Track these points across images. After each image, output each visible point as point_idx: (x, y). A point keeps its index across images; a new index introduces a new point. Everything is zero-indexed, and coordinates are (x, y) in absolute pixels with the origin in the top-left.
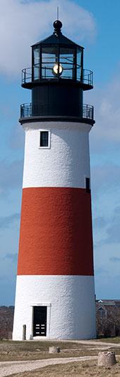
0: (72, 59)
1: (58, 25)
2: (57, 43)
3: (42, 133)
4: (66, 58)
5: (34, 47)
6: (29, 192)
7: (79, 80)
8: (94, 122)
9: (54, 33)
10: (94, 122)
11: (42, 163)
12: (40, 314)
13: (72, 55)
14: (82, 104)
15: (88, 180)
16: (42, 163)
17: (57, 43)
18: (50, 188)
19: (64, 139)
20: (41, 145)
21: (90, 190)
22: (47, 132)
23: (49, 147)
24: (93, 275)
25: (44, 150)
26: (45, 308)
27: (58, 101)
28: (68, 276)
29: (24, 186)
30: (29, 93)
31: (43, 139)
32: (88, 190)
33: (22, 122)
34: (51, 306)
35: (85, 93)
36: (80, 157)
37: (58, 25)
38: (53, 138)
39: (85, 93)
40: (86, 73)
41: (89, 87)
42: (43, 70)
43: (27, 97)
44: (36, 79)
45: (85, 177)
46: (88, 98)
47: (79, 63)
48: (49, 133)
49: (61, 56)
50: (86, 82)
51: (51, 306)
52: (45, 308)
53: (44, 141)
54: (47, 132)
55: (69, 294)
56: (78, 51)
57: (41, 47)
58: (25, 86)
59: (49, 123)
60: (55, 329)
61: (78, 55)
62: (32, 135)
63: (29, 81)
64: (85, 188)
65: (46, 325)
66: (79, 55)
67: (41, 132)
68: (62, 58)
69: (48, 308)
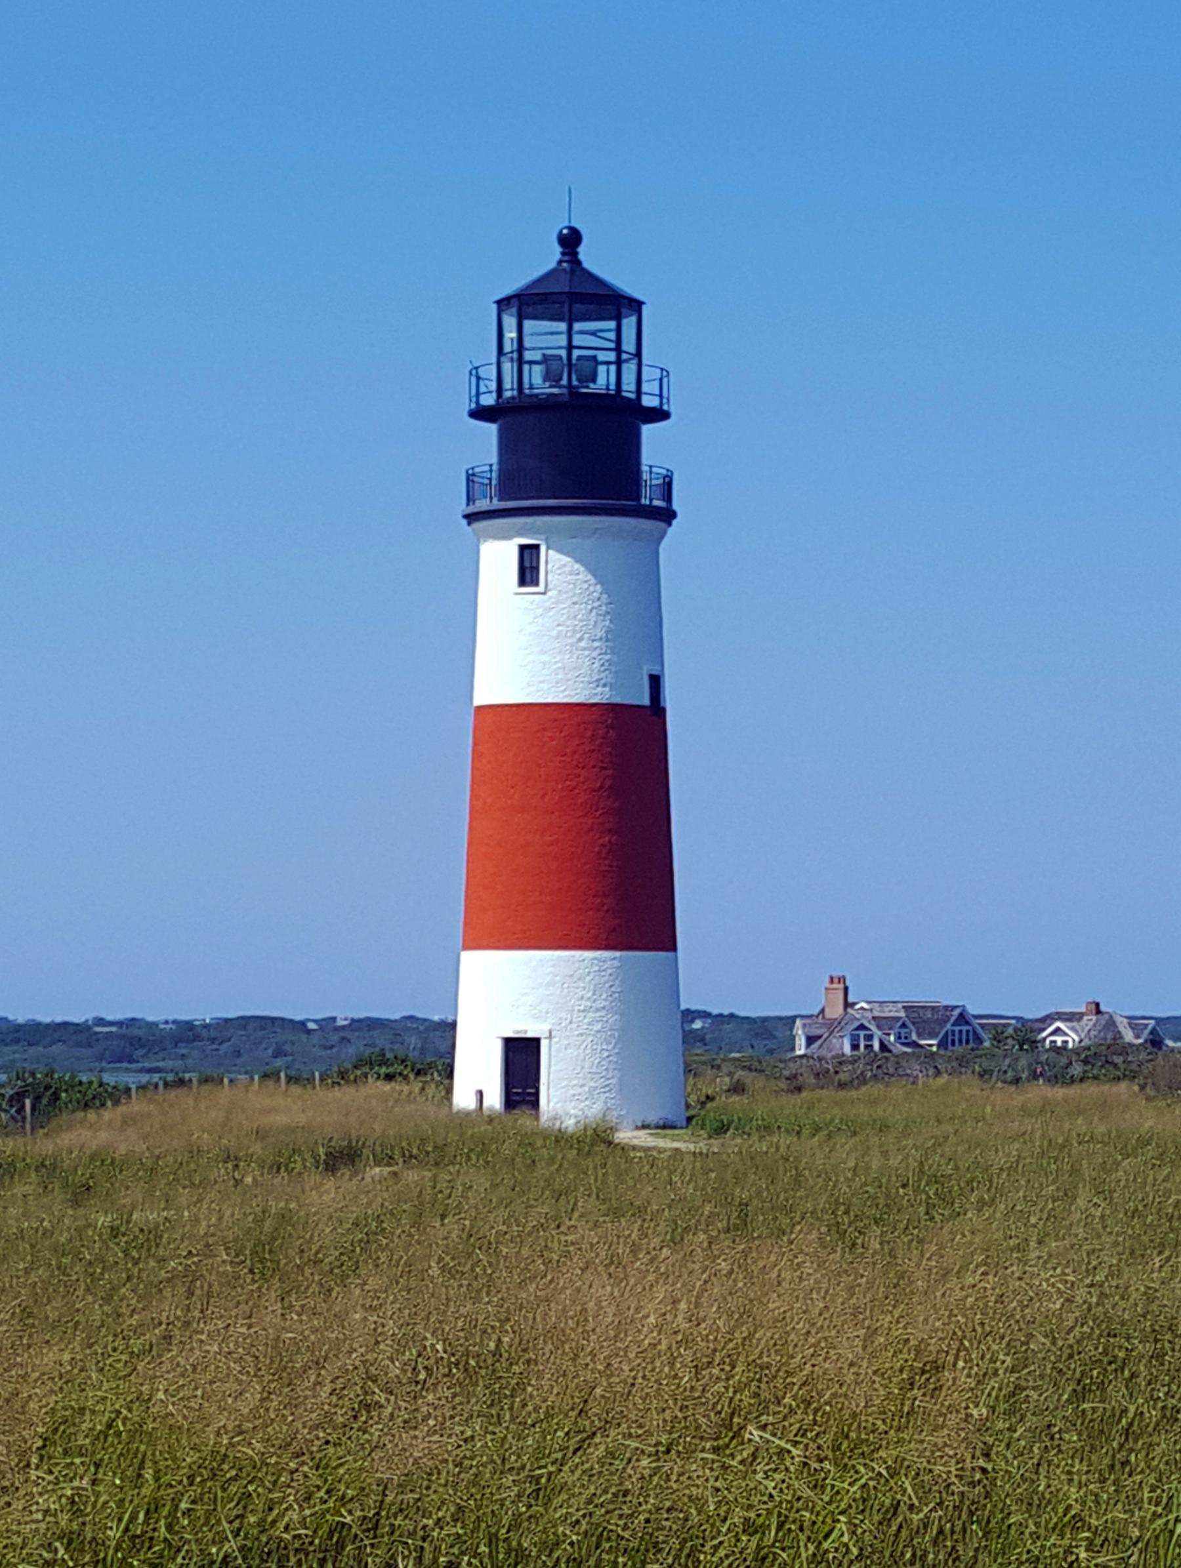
0: (612, 336)
1: (570, 240)
2: (573, 292)
3: (523, 548)
4: (593, 333)
5: (503, 304)
6: (501, 721)
7: (632, 396)
8: (673, 515)
9: (560, 262)
10: (673, 515)
11: (527, 633)
12: (521, 1057)
13: (612, 324)
14: (638, 463)
15: (656, 682)
16: (527, 633)
17: (573, 292)
18: (507, 705)
19: (600, 580)
20: (523, 582)
21: (664, 710)
22: (537, 547)
23: (541, 588)
24: (673, 948)
25: (529, 598)
26: (537, 1041)
27: (575, 454)
28: (618, 954)
29: (482, 697)
30: (491, 430)
31: (527, 564)
32: (656, 709)
33: (471, 518)
34: (550, 1037)
35: (648, 431)
36: (635, 617)
37: (570, 240)
38: (552, 562)
39: (648, 431)
40: (646, 373)
41: (659, 414)
42: (526, 367)
43: (484, 445)
44: (508, 394)
45: (646, 670)
46: (656, 447)
47: (629, 345)
48: (543, 549)
49: (577, 326)
50: (649, 401)
51: (550, 1037)
52: (537, 1041)
53: (528, 573)
54: (537, 547)
55: (600, 1004)
56: (624, 311)
57: (526, 303)
58: (480, 414)
59: (530, 520)
60: (564, 1098)
61: (625, 322)
62: (498, 556)
63: (488, 400)
64: (646, 701)
65: (538, 1089)
66: (629, 324)
67: (523, 548)
68: (581, 332)
69: (544, 1044)
